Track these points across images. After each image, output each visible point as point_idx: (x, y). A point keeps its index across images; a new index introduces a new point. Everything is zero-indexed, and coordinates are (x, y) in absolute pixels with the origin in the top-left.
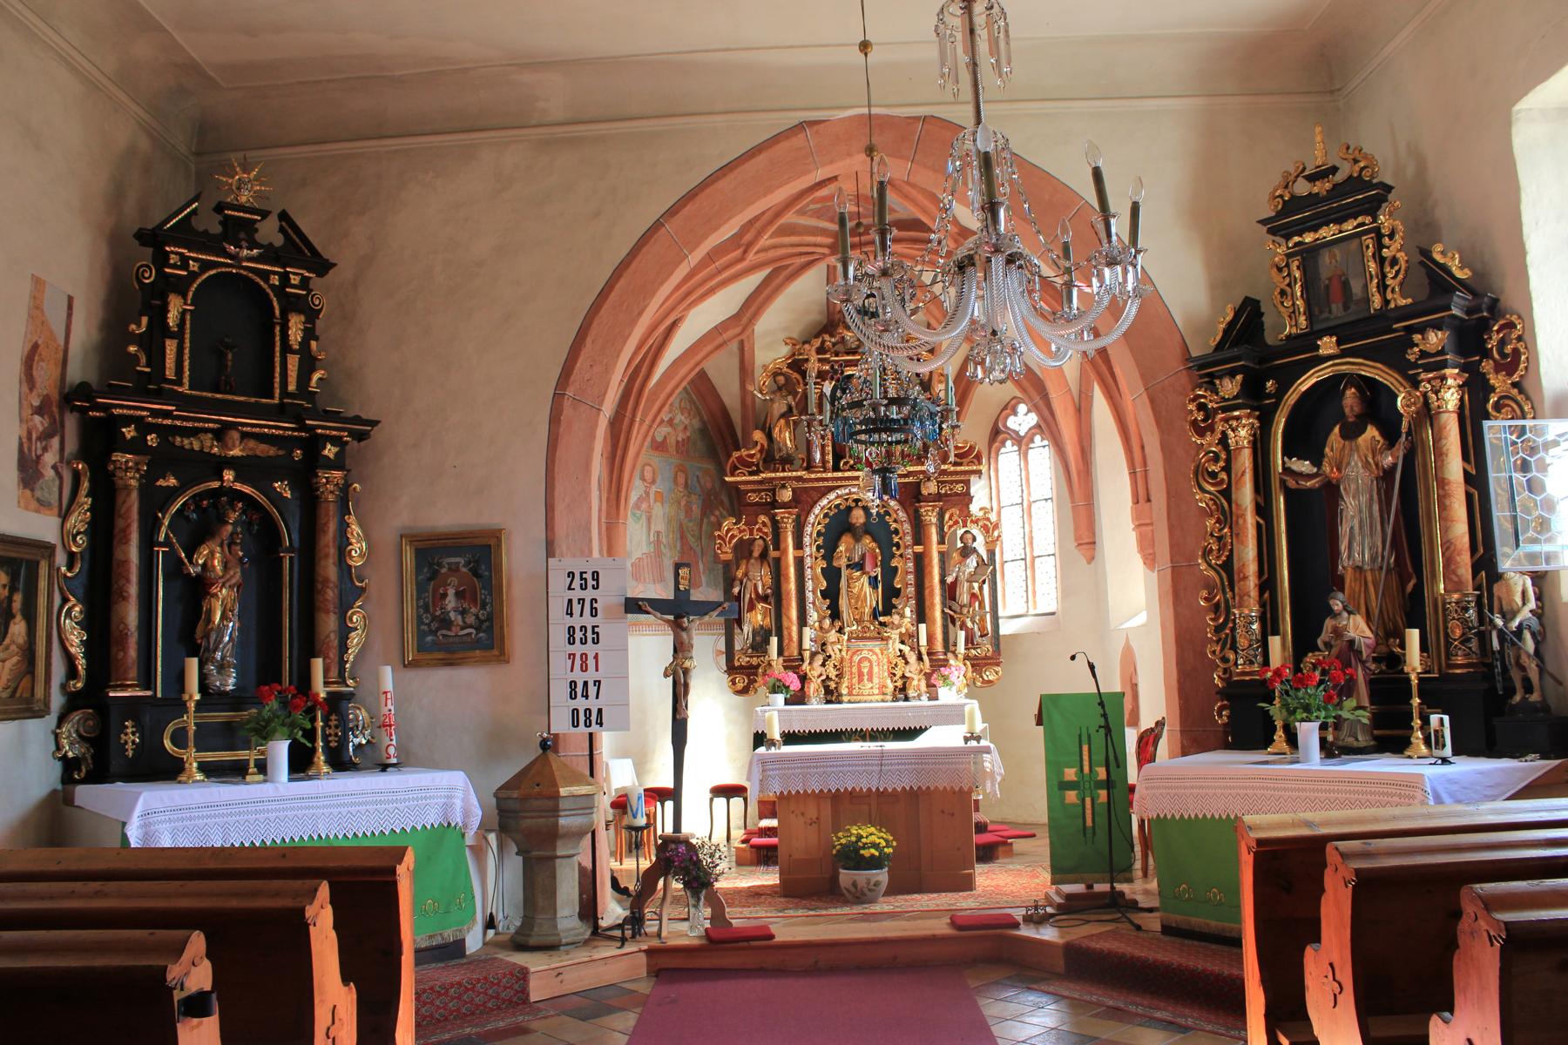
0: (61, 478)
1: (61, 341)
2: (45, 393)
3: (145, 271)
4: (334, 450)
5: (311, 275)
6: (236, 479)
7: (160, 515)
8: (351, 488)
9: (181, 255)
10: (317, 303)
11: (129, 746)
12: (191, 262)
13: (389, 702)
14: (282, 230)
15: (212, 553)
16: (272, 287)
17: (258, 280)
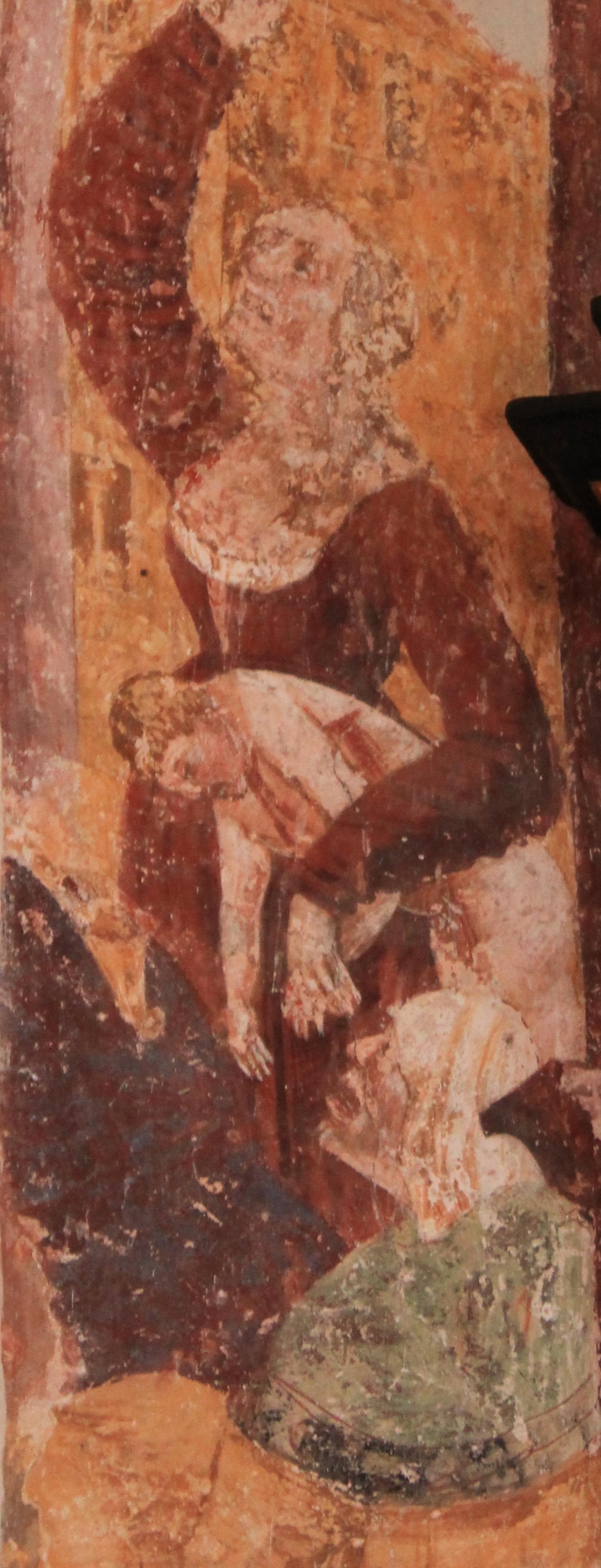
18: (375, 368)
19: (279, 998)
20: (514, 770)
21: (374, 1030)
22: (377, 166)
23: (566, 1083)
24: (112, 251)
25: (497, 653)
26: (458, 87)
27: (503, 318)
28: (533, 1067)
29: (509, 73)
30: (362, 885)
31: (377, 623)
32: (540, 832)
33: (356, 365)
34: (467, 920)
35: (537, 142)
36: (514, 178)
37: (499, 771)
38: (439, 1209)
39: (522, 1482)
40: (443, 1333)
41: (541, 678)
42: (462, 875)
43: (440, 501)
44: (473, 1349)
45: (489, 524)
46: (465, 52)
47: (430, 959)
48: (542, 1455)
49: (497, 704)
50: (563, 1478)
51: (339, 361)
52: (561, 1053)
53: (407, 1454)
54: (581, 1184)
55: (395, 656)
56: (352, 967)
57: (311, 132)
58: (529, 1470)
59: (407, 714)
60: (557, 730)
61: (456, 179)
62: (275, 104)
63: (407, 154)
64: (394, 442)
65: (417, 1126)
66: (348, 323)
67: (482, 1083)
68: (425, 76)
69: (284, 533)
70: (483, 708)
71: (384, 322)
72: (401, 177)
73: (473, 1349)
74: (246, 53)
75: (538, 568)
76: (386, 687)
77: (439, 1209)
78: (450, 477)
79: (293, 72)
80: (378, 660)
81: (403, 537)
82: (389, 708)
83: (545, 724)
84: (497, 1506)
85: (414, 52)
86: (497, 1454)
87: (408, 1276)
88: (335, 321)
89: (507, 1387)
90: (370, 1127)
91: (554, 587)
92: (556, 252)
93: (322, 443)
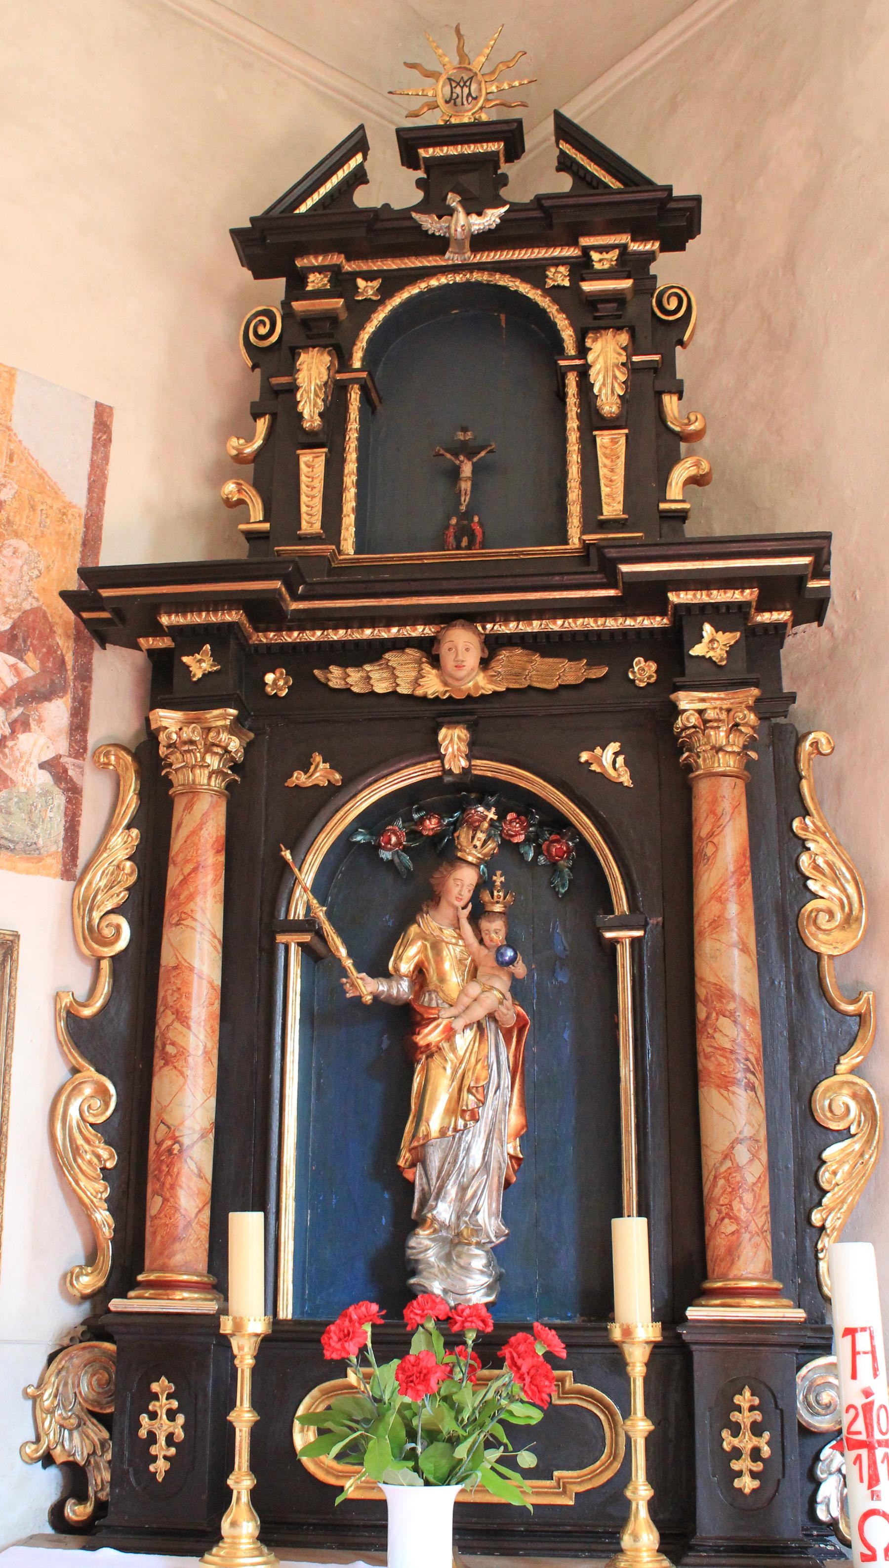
0: (73, 793)
1: (79, 497)
2: (27, 606)
3: (263, 323)
4: (727, 639)
5: (648, 247)
6: (475, 749)
7: (287, 855)
8: (806, 746)
9: (335, 272)
10: (673, 305)
11: (160, 1449)
12: (361, 283)
13: (864, 1363)
14: (565, 164)
15: (436, 946)
16: (555, 293)
17: (524, 289)
18: (31, 579)
19: (69, 801)
20: (57, 681)
21: (13, 740)
22: (36, 529)
23: (62, 760)
24: (507, 958)
25: (56, 652)
26: (60, 511)
27: (66, 568)
28: (54, 755)
29: (74, 507)
30: (14, 705)
31: (25, 641)
32: (62, 697)
33: (26, 578)
34: (39, 716)
35: (80, 524)
36: (73, 533)
37: (52, 681)
38: (25, 785)
39: (40, 854)
40: (23, 815)
41: (67, 659)
42: (40, 705)
43: (45, 614)
44: (30, 820)
45: (57, 620)
46: (63, 502)
47: (29, 725)
48: (46, 849)
49: (54, 664)
50: (51, 855)
51: (22, 577)
52: (61, 752)
53: (12, 841)
54: (63, 785)
55: (29, 650)
56: (9, 724)
57: (20, 521)
58: (42, 851)
59: (30, 664)
60: (69, 672)
61: (57, 533)
62: (12, 514)
63: (44, 527)
64: (34, 598)
65: (22, 764)
66: (25, 568)
67: (39, 757)
68: (51, 507)
69: (3, 618)
70: (50, 665)
71: (34, 568)
72: (42, 532)
73: (30, 820)
74: (5, 501)
75: (69, 632)
76: (25, 657)
77: (25, 785)
78: (48, 607)
79: (17, 506)
80: (24, 651)
81: (33, 621)
82: (26, 662)
83: (66, 671)
84: (33, 858)
85: (49, 502)
86: (34, 846)
87: (16, 800)
88: (22, 567)
89: (38, 831)
90: (10, 763)
91: (73, 637)
92: (83, 552)
93: (15, 597)
